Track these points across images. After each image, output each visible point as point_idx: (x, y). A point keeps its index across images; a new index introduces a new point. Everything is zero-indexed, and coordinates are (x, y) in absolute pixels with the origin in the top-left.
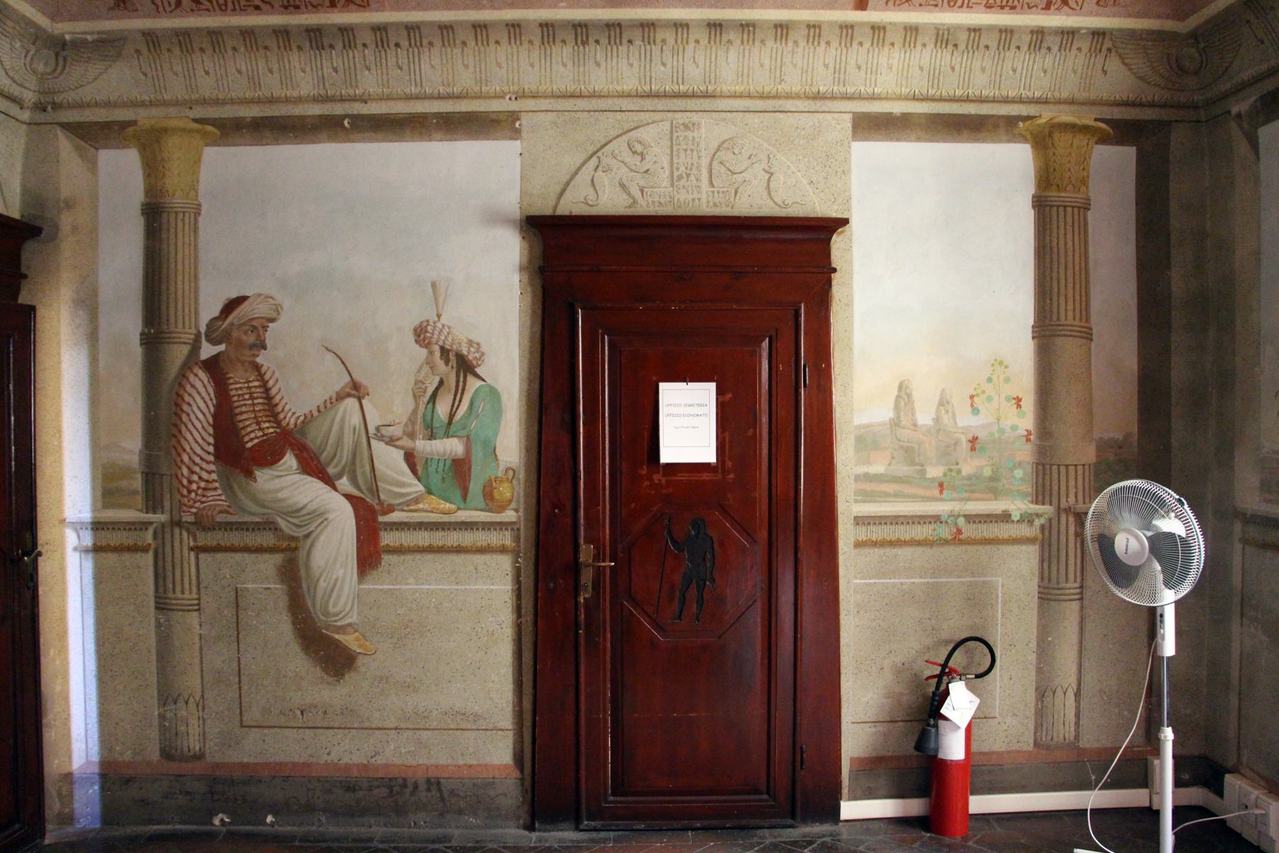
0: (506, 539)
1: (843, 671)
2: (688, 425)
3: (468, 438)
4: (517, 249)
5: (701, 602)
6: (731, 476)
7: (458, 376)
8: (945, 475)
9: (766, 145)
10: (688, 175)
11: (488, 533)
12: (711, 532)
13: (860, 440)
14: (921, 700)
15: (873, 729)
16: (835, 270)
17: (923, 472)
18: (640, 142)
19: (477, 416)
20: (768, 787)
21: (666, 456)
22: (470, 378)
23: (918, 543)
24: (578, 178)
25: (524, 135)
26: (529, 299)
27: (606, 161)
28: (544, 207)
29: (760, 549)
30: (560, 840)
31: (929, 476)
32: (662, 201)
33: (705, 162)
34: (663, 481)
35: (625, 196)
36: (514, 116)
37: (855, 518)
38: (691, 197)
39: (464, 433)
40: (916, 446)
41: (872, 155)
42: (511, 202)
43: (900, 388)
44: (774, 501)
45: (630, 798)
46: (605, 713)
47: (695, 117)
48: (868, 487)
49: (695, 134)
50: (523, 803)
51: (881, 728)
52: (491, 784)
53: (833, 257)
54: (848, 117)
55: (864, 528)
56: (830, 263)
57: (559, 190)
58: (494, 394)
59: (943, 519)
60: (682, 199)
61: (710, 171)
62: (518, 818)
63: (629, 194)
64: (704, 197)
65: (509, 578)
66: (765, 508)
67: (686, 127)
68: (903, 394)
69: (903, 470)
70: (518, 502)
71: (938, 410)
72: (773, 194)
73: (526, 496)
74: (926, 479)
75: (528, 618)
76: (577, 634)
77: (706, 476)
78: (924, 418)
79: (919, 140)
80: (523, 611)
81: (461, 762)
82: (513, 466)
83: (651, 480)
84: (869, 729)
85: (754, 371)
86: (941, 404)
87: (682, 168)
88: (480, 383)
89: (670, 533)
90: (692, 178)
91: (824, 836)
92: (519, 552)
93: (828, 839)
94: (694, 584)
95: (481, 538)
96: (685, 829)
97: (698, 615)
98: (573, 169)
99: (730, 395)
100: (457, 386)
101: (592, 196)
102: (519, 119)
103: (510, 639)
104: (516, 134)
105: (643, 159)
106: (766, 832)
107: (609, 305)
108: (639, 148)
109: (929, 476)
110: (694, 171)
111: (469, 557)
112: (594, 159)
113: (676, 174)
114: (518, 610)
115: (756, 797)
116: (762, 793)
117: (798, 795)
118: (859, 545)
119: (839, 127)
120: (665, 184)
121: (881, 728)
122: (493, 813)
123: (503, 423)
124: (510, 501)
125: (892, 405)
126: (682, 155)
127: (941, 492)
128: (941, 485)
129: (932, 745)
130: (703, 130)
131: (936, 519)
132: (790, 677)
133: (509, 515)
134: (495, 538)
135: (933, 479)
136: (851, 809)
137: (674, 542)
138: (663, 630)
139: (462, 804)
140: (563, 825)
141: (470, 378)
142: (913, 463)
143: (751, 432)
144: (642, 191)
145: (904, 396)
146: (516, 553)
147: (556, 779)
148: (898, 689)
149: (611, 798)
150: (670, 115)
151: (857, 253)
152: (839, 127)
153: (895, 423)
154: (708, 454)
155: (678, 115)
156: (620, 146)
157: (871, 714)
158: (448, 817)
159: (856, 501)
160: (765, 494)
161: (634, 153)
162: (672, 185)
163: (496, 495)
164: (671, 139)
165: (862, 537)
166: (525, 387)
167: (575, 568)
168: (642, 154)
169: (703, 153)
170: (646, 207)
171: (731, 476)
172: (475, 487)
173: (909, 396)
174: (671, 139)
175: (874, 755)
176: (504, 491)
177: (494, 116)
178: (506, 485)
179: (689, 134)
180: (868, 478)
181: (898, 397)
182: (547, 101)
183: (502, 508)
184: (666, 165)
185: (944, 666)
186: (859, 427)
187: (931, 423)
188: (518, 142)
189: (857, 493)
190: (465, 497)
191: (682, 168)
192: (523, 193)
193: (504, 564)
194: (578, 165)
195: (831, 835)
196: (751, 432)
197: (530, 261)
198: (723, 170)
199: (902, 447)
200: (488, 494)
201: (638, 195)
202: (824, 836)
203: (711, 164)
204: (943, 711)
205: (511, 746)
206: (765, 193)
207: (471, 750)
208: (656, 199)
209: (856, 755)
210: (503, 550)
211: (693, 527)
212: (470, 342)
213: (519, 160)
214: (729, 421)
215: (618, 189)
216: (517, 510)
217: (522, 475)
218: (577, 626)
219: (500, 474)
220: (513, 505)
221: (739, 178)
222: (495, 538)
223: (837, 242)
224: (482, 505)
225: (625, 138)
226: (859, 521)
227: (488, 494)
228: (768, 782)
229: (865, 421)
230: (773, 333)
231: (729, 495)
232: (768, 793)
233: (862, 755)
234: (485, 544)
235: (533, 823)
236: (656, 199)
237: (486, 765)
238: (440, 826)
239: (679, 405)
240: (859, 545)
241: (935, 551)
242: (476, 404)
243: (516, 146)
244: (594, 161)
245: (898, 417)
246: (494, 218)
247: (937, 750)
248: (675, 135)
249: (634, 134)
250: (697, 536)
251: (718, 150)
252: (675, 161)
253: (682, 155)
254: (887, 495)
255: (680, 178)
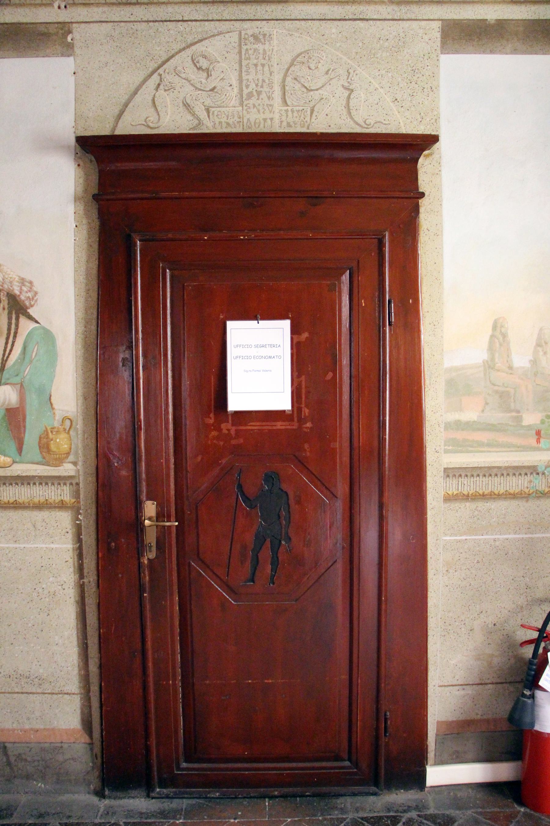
0: (65, 494)
1: (430, 633)
2: (259, 368)
3: (22, 385)
4: (73, 177)
5: (275, 563)
6: (309, 425)
7: (10, 318)
8: (542, 422)
9: (345, 58)
10: (259, 93)
11: (45, 488)
12: (284, 486)
13: (451, 384)
14: (513, 661)
15: (462, 692)
16: (422, 195)
17: (519, 419)
18: (205, 57)
19: (31, 362)
20: (350, 752)
21: (235, 403)
22: (23, 320)
23: (513, 496)
24: (138, 98)
25: (77, 51)
26: (85, 232)
27: (169, 78)
28: (101, 128)
29: (339, 506)
30: (130, 813)
31: (525, 423)
32: (231, 121)
33: (277, 78)
34: (233, 432)
35: (190, 117)
36: (65, 28)
37: (445, 470)
38: (262, 116)
39: (17, 380)
40: (512, 391)
41: (464, 69)
42: (67, 128)
43: (495, 327)
44: (356, 452)
45: (205, 765)
46: (174, 680)
47: (266, 27)
48: (459, 435)
49: (267, 47)
50: (93, 768)
51: (469, 691)
52: (58, 749)
53: (420, 182)
54: (437, 25)
55: (455, 481)
56: (417, 187)
57: (117, 112)
58: (48, 337)
59: (540, 470)
60: (252, 120)
61: (283, 87)
62: (89, 785)
63: (193, 114)
64: (277, 117)
65: (70, 536)
66: (346, 459)
67: (256, 38)
68: (497, 333)
69: (496, 416)
70: (76, 454)
71: (535, 352)
72: (353, 112)
73: (85, 447)
74: (523, 427)
75: (91, 578)
76: (141, 598)
77: (279, 425)
78: (521, 360)
79: (515, 51)
80: (86, 571)
81: (27, 727)
82: (70, 415)
83: (220, 430)
84: (457, 692)
85: (333, 309)
86: (538, 345)
87: (253, 86)
88: (33, 325)
89: (240, 487)
90: (263, 96)
91: (408, 809)
92: (79, 509)
93: (413, 814)
94: (268, 543)
95: (39, 493)
96: (263, 797)
97: (272, 577)
98: (133, 88)
99: (305, 335)
100: (9, 329)
101: (153, 117)
102: (70, 32)
103: (73, 600)
104: (68, 49)
105: (209, 75)
106: (349, 800)
107: (170, 236)
108: (204, 63)
109: (525, 423)
110: (266, 89)
111: (26, 513)
112: (155, 77)
113: (245, 92)
114: (80, 570)
115: (336, 764)
116: (343, 760)
117: (382, 763)
118: (449, 499)
119: (426, 38)
120: (233, 103)
121: (469, 691)
122: (62, 779)
123: (58, 368)
124: (68, 454)
125: (485, 345)
126: (252, 70)
127: (538, 441)
128: (538, 433)
129: (527, 720)
130: (275, 42)
131: (533, 470)
132: (375, 577)
133: (68, 469)
134: (53, 493)
135: (529, 427)
136: (437, 775)
137: (246, 499)
138: (234, 592)
139: (30, 769)
140: (134, 793)
141: (23, 320)
142: (509, 410)
143: (330, 375)
144: (208, 111)
145: (499, 335)
146: (76, 510)
147: (129, 745)
148: (488, 651)
149: (184, 765)
150: (237, 24)
151: (447, 176)
152: (426, 38)
153: (489, 366)
154: (283, 402)
155: (247, 25)
156: (183, 60)
157: (460, 677)
158: (17, 781)
159: (446, 451)
160: (346, 444)
161: (200, 69)
162: (241, 104)
163: (53, 447)
164: (240, 52)
165: (453, 491)
166: (81, 329)
167: (137, 527)
168: (207, 70)
169: (275, 68)
170: (211, 126)
171: (309, 425)
172: (31, 438)
173: (504, 336)
174: (240, 52)
175: (462, 718)
176: (61, 443)
177: (42, 29)
178: (63, 436)
179: (260, 47)
180: (459, 425)
181: (492, 336)
182: (100, 9)
183: (59, 461)
184: (235, 83)
185: (542, 630)
186: (450, 370)
187: (528, 365)
188: (72, 58)
189: (448, 442)
190: (20, 450)
191: (253, 86)
192: (78, 117)
193: (65, 519)
194: (137, 83)
195: (417, 808)
196: (330, 375)
197: (86, 191)
198: (298, 86)
199: (497, 392)
200: (44, 446)
201: (203, 115)
202: (408, 809)
203: (284, 81)
204: (540, 683)
205: (79, 711)
206: (345, 112)
207: (37, 714)
208: (224, 120)
209: (444, 719)
210: (62, 506)
211: (266, 480)
212: (23, 281)
213: (72, 79)
214: (304, 360)
215: (182, 109)
216: (75, 464)
217: (80, 425)
218: (141, 590)
219: (56, 424)
220: (71, 458)
221: (316, 95)
222: (53, 493)
223: (424, 164)
224: (39, 458)
225: (189, 52)
226: (450, 473)
227: (44, 446)
228: (350, 746)
229: (457, 363)
230: (354, 264)
231: (306, 446)
232: (350, 760)
233: (450, 719)
234: (42, 500)
235: (103, 789)
236: (224, 120)
237: (53, 729)
238: (9, 792)
239: (249, 346)
240: (449, 499)
241: (532, 504)
242: (30, 347)
243: (67, 64)
244: (155, 78)
245: (493, 359)
246: (46, 144)
247: (533, 724)
248: (244, 47)
249: (199, 48)
250: (270, 491)
251: (292, 64)
252: (245, 77)
253: (252, 70)
254: (481, 444)
255: (250, 96)
